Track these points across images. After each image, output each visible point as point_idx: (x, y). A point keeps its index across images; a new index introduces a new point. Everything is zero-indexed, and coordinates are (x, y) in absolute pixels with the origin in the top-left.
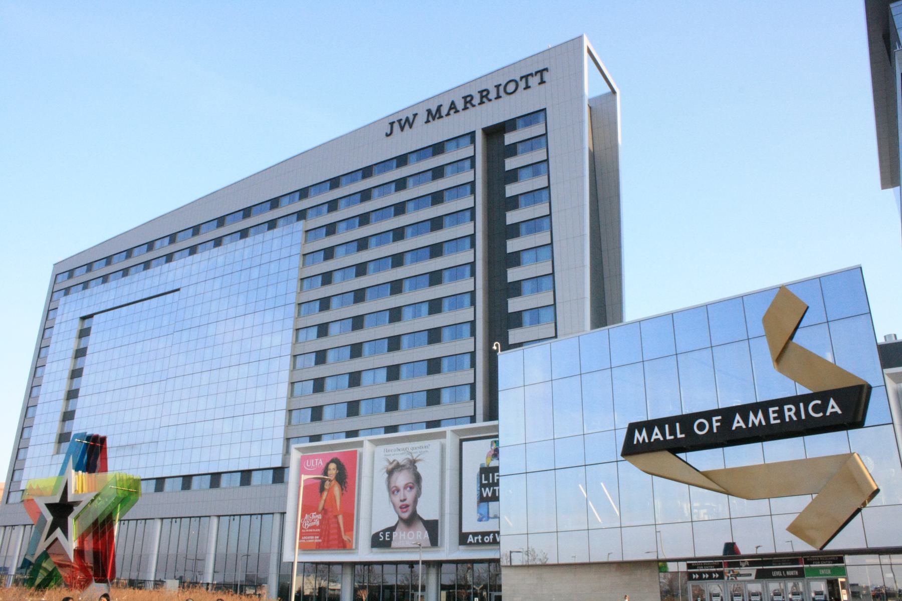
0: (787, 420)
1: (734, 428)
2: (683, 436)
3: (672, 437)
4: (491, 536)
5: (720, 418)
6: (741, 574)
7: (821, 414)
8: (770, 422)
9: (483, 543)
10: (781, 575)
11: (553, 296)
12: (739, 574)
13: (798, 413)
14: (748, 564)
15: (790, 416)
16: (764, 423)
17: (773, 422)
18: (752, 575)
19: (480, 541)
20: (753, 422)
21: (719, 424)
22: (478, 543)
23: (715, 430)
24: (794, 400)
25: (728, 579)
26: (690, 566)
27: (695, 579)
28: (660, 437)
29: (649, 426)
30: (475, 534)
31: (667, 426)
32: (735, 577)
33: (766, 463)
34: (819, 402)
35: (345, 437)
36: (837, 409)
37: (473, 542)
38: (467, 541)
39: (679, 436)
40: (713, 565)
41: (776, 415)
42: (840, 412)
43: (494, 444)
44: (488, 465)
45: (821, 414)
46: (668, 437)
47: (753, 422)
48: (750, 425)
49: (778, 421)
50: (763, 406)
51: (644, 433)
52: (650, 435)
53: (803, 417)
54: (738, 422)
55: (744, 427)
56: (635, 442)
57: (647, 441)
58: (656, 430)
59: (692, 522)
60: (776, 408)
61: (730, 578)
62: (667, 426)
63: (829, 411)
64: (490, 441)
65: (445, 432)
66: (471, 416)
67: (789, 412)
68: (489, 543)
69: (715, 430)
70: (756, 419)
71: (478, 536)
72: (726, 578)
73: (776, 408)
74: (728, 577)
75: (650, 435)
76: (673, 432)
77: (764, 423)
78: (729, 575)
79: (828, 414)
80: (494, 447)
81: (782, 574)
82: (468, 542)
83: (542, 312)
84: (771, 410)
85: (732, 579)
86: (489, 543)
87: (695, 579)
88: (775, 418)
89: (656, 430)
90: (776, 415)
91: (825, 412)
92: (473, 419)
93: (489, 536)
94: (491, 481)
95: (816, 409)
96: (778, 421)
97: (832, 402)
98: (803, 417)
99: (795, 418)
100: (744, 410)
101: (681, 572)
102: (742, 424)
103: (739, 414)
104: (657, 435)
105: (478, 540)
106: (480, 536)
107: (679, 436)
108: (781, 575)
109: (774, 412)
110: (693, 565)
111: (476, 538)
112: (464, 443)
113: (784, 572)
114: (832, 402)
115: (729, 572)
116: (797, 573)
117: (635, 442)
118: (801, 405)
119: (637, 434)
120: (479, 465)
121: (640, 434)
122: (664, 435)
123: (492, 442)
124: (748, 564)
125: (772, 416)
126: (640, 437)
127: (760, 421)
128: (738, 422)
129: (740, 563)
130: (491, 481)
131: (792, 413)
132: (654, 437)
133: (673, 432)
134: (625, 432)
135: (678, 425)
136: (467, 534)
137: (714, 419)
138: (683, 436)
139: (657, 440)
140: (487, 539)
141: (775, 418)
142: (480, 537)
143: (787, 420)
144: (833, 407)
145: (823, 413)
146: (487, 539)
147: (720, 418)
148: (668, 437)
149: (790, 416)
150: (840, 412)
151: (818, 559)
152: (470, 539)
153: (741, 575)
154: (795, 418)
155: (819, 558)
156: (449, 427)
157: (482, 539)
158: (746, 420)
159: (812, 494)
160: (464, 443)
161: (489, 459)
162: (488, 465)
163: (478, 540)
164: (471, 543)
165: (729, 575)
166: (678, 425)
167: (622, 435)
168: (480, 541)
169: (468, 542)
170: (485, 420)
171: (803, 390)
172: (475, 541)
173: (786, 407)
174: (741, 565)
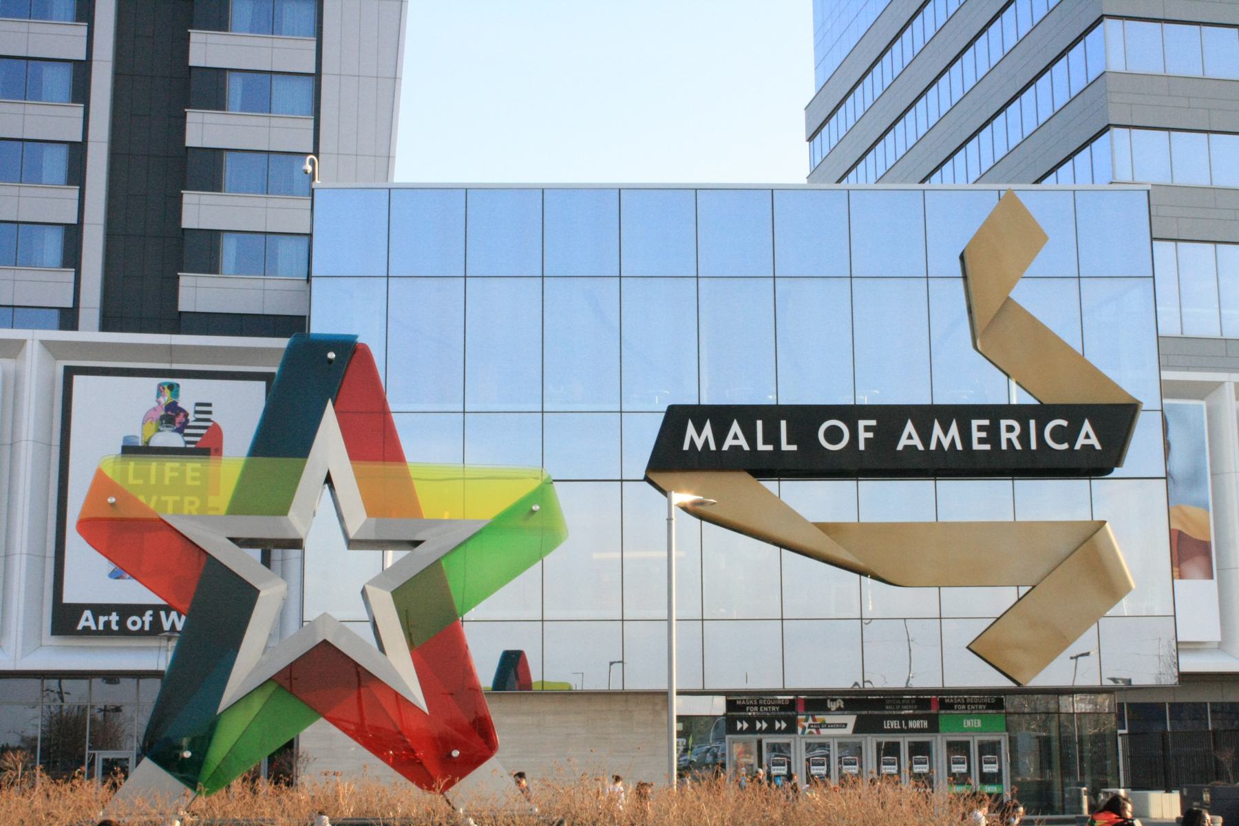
0: (1004, 446)
1: (900, 447)
2: (794, 448)
3: (770, 448)
4: (148, 617)
5: (873, 423)
6: (827, 725)
7: (1065, 446)
8: (972, 447)
9: (124, 632)
10: (899, 727)
11: (314, 53)
12: (825, 724)
13: (1024, 439)
14: (842, 706)
15: (1009, 441)
16: (959, 447)
17: (976, 446)
18: (848, 726)
19: (115, 627)
20: (939, 442)
21: (870, 435)
22: (107, 631)
23: (862, 447)
24: (1019, 413)
25: (803, 732)
26: (731, 705)
27: (741, 732)
28: (742, 442)
29: (721, 416)
30: (99, 610)
31: (759, 423)
32: (817, 729)
33: (1018, 519)
34: (1064, 423)
35: (98, 329)
36: (1094, 441)
37: (93, 627)
38: (77, 623)
39: (785, 447)
40: (984, 704)
41: (984, 435)
42: (1098, 447)
43: (167, 392)
44: (147, 443)
45: (1065, 446)
46: (761, 447)
47: (939, 442)
48: (933, 446)
49: (987, 447)
50: (962, 414)
51: (708, 430)
52: (720, 436)
53: (1034, 446)
54: (909, 437)
55: (921, 447)
56: (686, 447)
57: (713, 447)
58: (735, 428)
59: (782, 619)
60: (986, 422)
61: (807, 731)
62: (759, 423)
63: (1081, 441)
64: (155, 382)
65: (21, 344)
66: (62, 310)
67: (1010, 433)
68: (141, 633)
69: (862, 447)
70: (946, 437)
71: (109, 614)
72: (800, 730)
73: (986, 422)
74: (804, 728)
75: (720, 436)
76: (772, 436)
77: (959, 447)
78: (806, 725)
79: (1077, 447)
80: (166, 398)
81: (901, 725)
82: (80, 627)
83: (279, 85)
84: (975, 423)
85: (811, 733)
86: (141, 633)
87: (741, 732)
88: (981, 441)
89: (735, 428)
90: (984, 435)
91: (1072, 442)
92: (69, 318)
93: (141, 615)
94: (153, 481)
95: (1058, 434)
96: (987, 447)
97: (1087, 427)
98: (1034, 446)
99: (1018, 446)
100: (925, 416)
101: (1077, 714)
102: (917, 442)
103: (912, 421)
104: (735, 437)
105: (107, 624)
106: (114, 614)
107: (785, 447)
108: (899, 727)
109: (980, 428)
110: (738, 703)
111: (102, 619)
112: (78, 380)
113: (903, 722)
114: (1087, 427)
115: (806, 720)
116: (925, 724)
117: (686, 447)
118: (1032, 423)
119: (691, 430)
120: (122, 439)
121: (699, 431)
122: (751, 440)
123: (160, 385)
124: (842, 706)
125: (976, 435)
126: (698, 437)
127: (953, 442)
128: (909, 437)
129: (828, 701)
130: (153, 481)
131: (1014, 436)
132: (729, 442)
133: (772, 436)
134: (655, 424)
135: (783, 424)
136: (78, 609)
137: (862, 423)
138: (794, 448)
139: (736, 449)
140: (134, 623)
141: (981, 441)
142: (114, 618)
143: (1004, 446)
144: (1088, 437)
145: (1069, 444)
146: (134, 623)
147: (873, 423)
148: (761, 447)
149: (1009, 441)
150: (1098, 447)
151: (963, 701)
152: (86, 620)
153: (827, 726)
154: (1018, 446)
155: (965, 699)
156: (37, 332)
157: (121, 623)
158: (925, 436)
159: (1018, 586)
160: (78, 380)
161: (152, 427)
162: (147, 443)
163: (107, 624)
164: (87, 631)
165: (806, 725)
166: (783, 424)
167: (652, 427)
168: (115, 627)
169: (80, 627)
170: (105, 326)
171: (1018, 397)
172: (101, 627)
173: (1004, 423)
174: (829, 706)
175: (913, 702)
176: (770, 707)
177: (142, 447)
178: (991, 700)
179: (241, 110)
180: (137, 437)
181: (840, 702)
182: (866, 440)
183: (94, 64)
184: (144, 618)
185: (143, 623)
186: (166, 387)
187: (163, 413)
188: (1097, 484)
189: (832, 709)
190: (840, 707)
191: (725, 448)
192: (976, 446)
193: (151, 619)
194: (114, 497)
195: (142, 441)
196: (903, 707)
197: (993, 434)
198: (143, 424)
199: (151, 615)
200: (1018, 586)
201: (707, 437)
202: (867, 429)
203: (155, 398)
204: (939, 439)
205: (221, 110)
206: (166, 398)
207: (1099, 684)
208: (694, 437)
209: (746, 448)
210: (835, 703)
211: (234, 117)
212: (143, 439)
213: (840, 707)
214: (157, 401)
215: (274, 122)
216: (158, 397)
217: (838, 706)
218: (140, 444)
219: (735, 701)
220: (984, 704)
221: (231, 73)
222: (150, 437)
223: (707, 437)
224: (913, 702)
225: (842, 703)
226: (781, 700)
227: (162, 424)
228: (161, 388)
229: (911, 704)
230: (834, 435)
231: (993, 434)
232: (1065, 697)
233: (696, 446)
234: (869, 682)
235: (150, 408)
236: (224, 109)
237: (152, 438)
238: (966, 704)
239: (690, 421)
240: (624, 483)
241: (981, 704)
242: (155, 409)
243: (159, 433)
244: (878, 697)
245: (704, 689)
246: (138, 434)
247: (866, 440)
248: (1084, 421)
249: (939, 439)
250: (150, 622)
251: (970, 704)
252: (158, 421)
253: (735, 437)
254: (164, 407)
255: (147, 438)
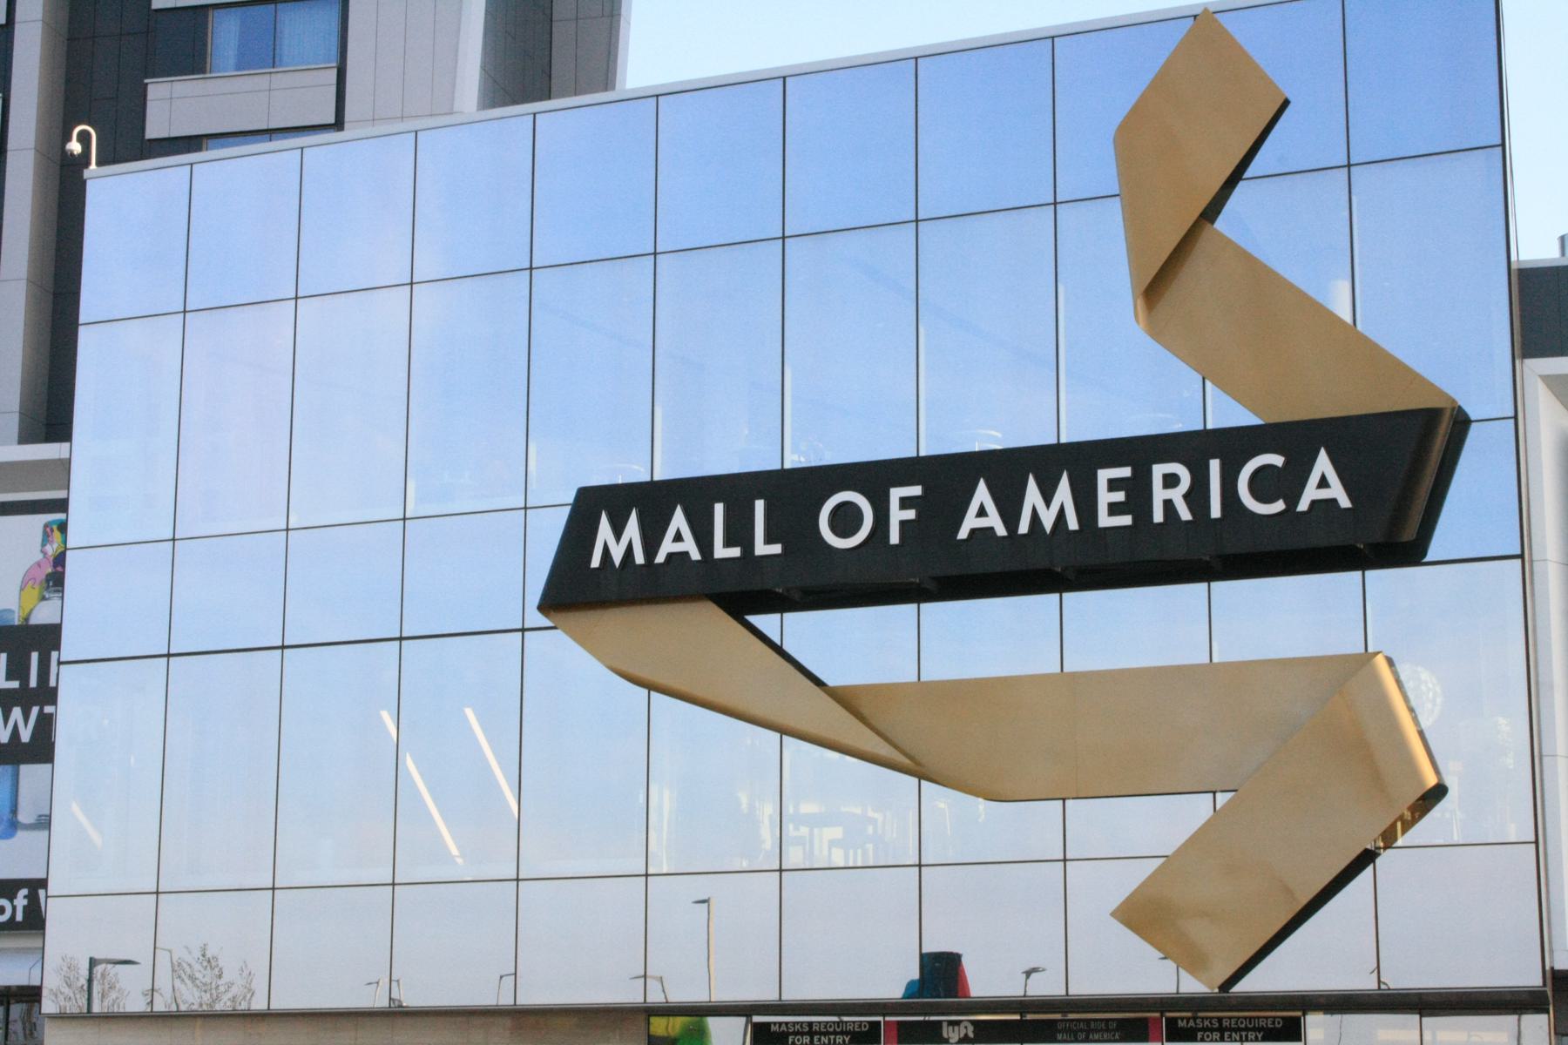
1: (963, 534)
2: (776, 549)
3: (735, 552)
4: (21, 900)
5: (916, 491)
7: (1279, 506)
13: (1198, 497)
14: (971, 1035)
15: (1168, 504)
17: (1105, 520)
21: (910, 514)
23: (894, 538)
28: (689, 546)
34: (1277, 460)
39: (761, 548)
41: (1119, 496)
42: (1345, 502)
43: (57, 535)
44: (27, 619)
45: (1279, 506)
46: (721, 552)
48: (1024, 528)
49: (1126, 520)
52: (651, 541)
53: (1216, 511)
55: (1001, 531)
56: (596, 562)
57: (639, 559)
58: (679, 520)
60: (1125, 472)
62: (719, 509)
63: (1311, 493)
69: (894, 538)
73: (1125, 472)
76: (739, 533)
77: (1073, 524)
88: (1114, 509)
89: (679, 520)
90: (1119, 496)
91: (1293, 499)
94: (33, 683)
95: (1263, 485)
96: (1126, 520)
97: (1323, 464)
98: (1216, 511)
99: (1185, 514)
102: (994, 521)
104: (679, 539)
107: (761, 548)
109: (1114, 485)
110: (773, 1028)
114: (1323, 464)
117: (596, 562)
118: (1215, 466)
119: (605, 530)
122: (704, 541)
123: (46, 526)
124: (971, 1035)
125: (1105, 497)
130: (33, 683)
131: (1177, 495)
132: (667, 547)
133: (739, 533)
135: (760, 505)
137: (896, 494)
138: (776, 549)
141: (1114, 509)
143: (1158, 517)
147: (916, 491)
149: (1168, 504)
150: (1345, 502)
154: (1185, 514)
155: (1220, 1020)
158: (1009, 507)
159: (1064, 800)
162: (27, 619)
166: (760, 505)
171: (1229, 413)
173: (1159, 471)
174: (945, 1035)
175: (1114, 1025)
176: (832, 1037)
177: (18, 627)
178: (1274, 1023)
179: (238, 69)
180: (13, 612)
181: (966, 1027)
182: (903, 524)
183: (17, 27)
184: (16, 902)
185: (14, 908)
186: (55, 527)
187: (50, 570)
188: (1381, 579)
189: (951, 1041)
190: (966, 1035)
191: (660, 558)
192: (1105, 520)
193: (25, 902)
194: (13, 706)
195: (19, 616)
196: (1091, 1037)
197: (1137, 494)
198: (22, 589)
199: (25, 897)
200: (1064, 800)
201: (605, 544)
202: (905, 503)
203: (39, 547)
204: (1034, 511)
205: (198, 73)
206: (55, 546)
207: (1063, 992)
208: (609, 544)
209: (695, 555)
210: (956, 1028)
211: (219, 81)
212: (21, 614)
213: (966, 1035)
214: (42, 551)
215: (280, 80)
216: (43, 545)
217: (962, 1035)
218: (16, 623)
219: (768, 1025)
220: (1259, 1029)
221: (217, 13)
222: (31, 610)
223: (605, 544)
224: (1114, 1025)
225: (971, 1028)
226: (820, 1023)
227: (48, 587)
228: (48, 530)
229: (1108, 1030)
230: (846, 520)
231: (1137, 494)
232: (75, 1010)
233: (611, 558)
234: (1384, 983)
235: (32, 563)
236: (204, 72)
237: (34, 612)
238: (811, 1033)
239: (603, 513)
240: (526, 633)
241: (842, 1033)
242: (39, 564)
243: (45, 602)
244: (921, 1018)
245: (780, 1000)
246: (15, 607)
247: (903, 524)
248: (1320, 449)
249: (1034, 511)
250: (24, 907)
251: (821, 1033)
252: (44, 582)
253: (679, 539)
254: (52, 559)
255: (27, 611)
